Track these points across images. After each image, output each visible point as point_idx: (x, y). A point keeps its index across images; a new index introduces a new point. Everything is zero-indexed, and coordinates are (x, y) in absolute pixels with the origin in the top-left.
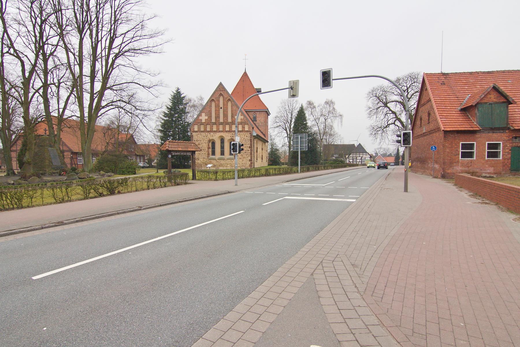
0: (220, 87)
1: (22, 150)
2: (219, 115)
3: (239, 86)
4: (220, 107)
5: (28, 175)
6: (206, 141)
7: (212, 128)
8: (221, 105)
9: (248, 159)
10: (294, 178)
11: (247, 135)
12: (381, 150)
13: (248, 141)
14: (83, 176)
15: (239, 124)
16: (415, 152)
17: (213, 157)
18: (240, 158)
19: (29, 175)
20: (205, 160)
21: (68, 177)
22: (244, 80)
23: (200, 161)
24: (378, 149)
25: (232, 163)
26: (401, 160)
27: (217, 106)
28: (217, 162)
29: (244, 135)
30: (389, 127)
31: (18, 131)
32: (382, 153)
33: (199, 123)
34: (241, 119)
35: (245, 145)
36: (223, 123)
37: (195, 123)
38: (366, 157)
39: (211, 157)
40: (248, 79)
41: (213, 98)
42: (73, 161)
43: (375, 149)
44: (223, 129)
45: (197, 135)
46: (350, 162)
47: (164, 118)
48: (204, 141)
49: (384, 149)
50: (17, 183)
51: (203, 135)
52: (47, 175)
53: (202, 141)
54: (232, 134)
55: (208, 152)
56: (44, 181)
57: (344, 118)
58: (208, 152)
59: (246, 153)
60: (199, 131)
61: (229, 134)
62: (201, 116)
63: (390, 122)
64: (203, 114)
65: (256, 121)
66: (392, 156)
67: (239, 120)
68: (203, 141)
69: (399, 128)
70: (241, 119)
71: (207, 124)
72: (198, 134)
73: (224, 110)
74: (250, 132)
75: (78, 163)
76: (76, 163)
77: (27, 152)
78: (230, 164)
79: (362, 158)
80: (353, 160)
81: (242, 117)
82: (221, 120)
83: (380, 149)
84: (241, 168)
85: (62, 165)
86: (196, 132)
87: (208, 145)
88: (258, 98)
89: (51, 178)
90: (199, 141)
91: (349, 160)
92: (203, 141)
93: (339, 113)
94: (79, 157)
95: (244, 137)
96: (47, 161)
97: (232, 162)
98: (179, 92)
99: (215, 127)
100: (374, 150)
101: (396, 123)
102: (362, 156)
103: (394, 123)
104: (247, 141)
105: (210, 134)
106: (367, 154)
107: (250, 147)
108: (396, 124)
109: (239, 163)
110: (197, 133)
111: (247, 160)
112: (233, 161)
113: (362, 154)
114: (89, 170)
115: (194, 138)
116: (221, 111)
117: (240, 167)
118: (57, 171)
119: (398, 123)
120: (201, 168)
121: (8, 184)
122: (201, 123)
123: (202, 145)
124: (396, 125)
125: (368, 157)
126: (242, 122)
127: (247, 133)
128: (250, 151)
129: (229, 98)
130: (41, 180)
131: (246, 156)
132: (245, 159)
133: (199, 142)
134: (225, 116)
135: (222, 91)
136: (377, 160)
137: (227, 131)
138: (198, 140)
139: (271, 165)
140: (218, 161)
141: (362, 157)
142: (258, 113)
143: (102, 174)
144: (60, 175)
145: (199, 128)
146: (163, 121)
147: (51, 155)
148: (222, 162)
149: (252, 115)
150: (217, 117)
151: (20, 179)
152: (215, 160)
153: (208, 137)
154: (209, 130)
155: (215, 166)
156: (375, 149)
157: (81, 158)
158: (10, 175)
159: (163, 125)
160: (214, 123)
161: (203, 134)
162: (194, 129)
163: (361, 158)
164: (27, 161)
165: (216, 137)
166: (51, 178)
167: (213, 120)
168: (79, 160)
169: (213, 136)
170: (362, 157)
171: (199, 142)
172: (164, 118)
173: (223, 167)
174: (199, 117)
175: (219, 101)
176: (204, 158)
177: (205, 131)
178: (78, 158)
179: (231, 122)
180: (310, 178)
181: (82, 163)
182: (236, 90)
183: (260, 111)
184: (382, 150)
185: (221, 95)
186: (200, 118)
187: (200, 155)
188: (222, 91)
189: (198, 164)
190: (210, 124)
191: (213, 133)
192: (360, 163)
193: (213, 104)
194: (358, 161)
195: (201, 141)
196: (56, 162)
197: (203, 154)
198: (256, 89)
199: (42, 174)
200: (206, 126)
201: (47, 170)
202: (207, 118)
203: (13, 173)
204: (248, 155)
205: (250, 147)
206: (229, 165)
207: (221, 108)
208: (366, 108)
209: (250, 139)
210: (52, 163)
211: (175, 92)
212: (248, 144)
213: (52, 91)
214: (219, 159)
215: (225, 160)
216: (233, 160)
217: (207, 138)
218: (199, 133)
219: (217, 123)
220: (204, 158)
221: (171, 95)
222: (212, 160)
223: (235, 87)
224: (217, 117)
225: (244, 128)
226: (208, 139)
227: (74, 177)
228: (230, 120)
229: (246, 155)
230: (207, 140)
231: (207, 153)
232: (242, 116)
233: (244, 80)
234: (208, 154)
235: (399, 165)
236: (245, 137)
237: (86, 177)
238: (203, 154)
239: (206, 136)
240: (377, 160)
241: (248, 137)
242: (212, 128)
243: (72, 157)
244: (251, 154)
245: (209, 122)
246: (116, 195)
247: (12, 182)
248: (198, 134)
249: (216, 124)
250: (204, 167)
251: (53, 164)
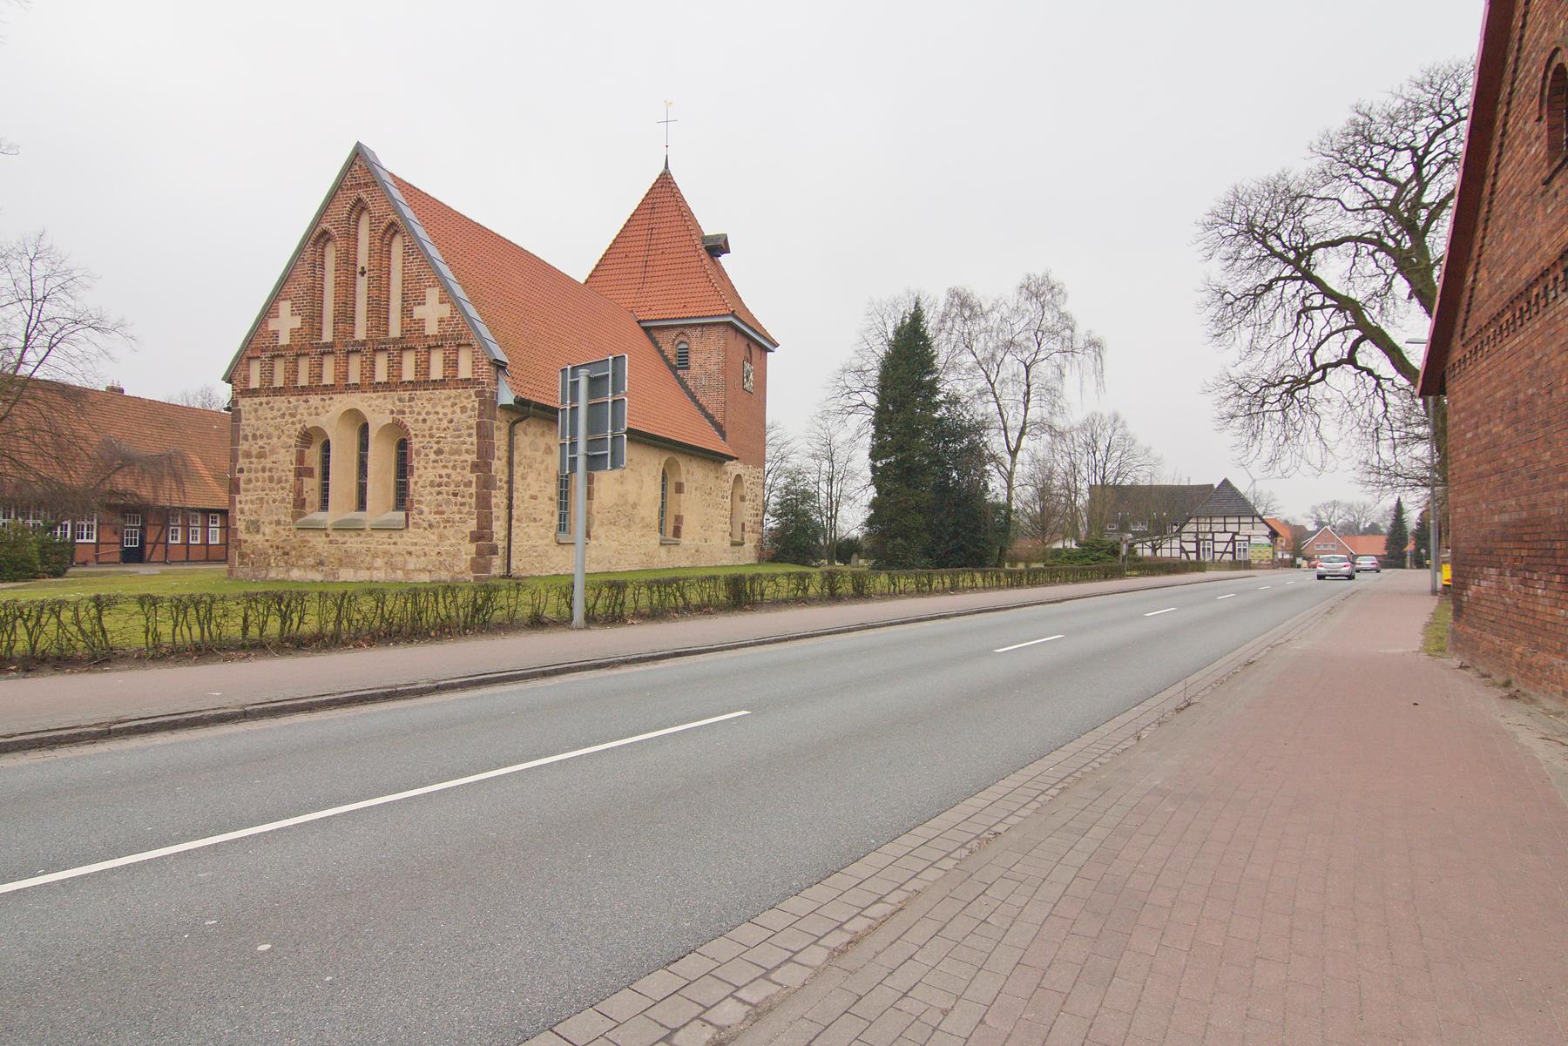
3: (632, 228)
4: (359, 270)
9: (467, 532)
10: (1148, 585)
12: (1336, 512)
13: (470, 435)
15: (430, 347)
16: (1498, 471)
17: (319, 516)
18: (431, 526)
20: (282, 532)
23: (264, 534)
24: (1325, 506)
26: (1410, 547)
27: (348, 260)
28: (331, 542)
29: (454, 405)
30: (1323, 378)
32: (1340, 521)
34: (441, 321)
35: (457, 457)
37: (249, 353)
38: (1254, 532)
43: (1313, 507)
45: (256, 410)
46: (1187, 553)
48: (284, 438)
49: (1350, 508)
51: (279, 410)
54: (400, 400)
55: (299, 492)
57: (1106, 356)
58: (299, 492)
61: (385, 398)
62: (277, 317)
63: (1323, 357)
64: (285, 307)
65: (688, 368)
66: (1381, 533)
67: (432, 329)
69: (1378, 384)
71: (298, 355)
72: (261, 404)
75: (171, 542)
79: (1237, 538)
80: (1198, 545)
81: (446, 310)
83: (1331, 510)
84: (435, 577)
86: (254, 393)
87: (301, 459)
91: (1183, 544)
92: (279, 437)
93: (1089, 332)
95: (448, 410)
97: (395, 543)
100: (1308, 512)
101: (1361, 359)
102: (1234, 528)
103: (1351, 360)
104: (465, 432)
105: (307, 401)
106: (1256, 520)
107: (475, 467)
108: (1360, 364)
109: (427, 549)
112: (399, 540)
113: (1236, 520)
115: (244, 422)
117: (430, 572)
119: (1371, 355)
122: (275, 348)
124: (1362, 369)
125: (1260, 535)
126: (443, 338)
128: (474, 485)
131: (460, 512)
132: (450, 532)
133: (261, 443)
134: (379, 309)
136: (1318, 546)
137: (376, 387)
138: (258, 433)
139: (775, 559)
140: (334, 536)
141: (1237, 533)
142: (697, 332)
148: (353, 543)
149: (668, 342)
152: (323, 534)
153: (298, 417)
155: (321, 563)
156: (1314, 509)
161: (280, 402)
163: (1233, 537)
165: (329, 414)
169: (317, 414)
170: (1237, 533)
171: (261, 443)
173: (356, 568)
177: (291, 389)
180: (919, 624)
181: (94, 541)
182: (619, 245)
183: (703, 325)
184: (1341, 513)
187: (265, 505)
189: (253, 553)
192: (1228, 557)
194: (1219, 547)
195: (269, 437)
197: (274, 501)
198: (704, 239)
205: (475, 467)
206: (379, 562)
208: (1206, 296)
209: (479, 425)
212: (467, 451)
214: (341, 528)
215: (364, 534)
218: (264, 400)
220: (278, 523)
222: (311, 533)
223: (618, 232)
224: (345, 315)
226: (298, 426)
229: (455, 509)
231: (291, 494)
234: (300, 503)
235: (1404, 567)
236: (453, 413)
239: (292, 415)
240: (1318, 546)
241: (469, 413)
244: (484, 502)
246: (96, 675)
248: (261, 404)
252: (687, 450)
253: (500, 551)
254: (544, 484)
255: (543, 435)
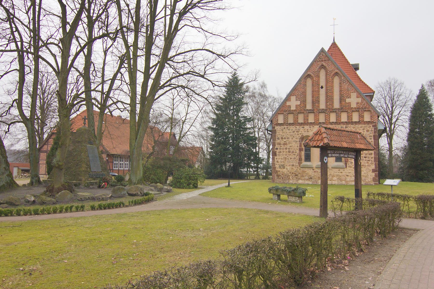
0: (321, 55)
1: (52, 149)
2: (318, 97)
5: (56, 186)
6: (297, 138)
7: (306, 118)
8: (322, 82)
11: (368, 129)
14: (135, 191)
15: (353, 111)
17: (308, 163)
19: (58, 186)
21: (114, 192)
22: (333, 54)
23: (287, 169)
25: (340, 174)
27: (316, 87)
28: (315, 172)
29: (363, 129)
31: (52, 129)
33: (286, 111)
34: (357, 103)
36: (326, 110)
37: (279, 112)
39: (304, 163)
40: (339, 52)
41: (309, 73)
42: (108, 165)
44: (326, 119)
45: (282, 130)
47: (216, 112)
48: (294, 139)
50: (40, 200)
51: (292, 130)
52: (82, 187)
53: (290, 139)
55: (300, 156)
56: (79, 199)
59: (367, 159)
60: (286, 123)
64: (293, 98)
68: (292, 139)
70: (357, 103)
73: (327, 90)
74: (374, 124)
75: (114, 169)
76: (111, 168)
77: (59, 150)
78: (337, 175)
82: (322, 106)
85: (102, 172)
88: (357, 77)
89: (88, 194)
90: (285, 138)
92: (292, 139)
94: (115, 161)
96: (84, 165)
97: (341, 172)
98: (236, 78)
99: (311, 118)
105: (303, 127)
110: (282, 127)
111: (368, 170)
112: (343, 171)
114: (138, 180)
115: (277, 133)
116: (323, 92)
118: (95, 181)
120: (287, 181)
121: (26, 202)
123: (290, 145)
127: (368, 126)
128: (373, 154)
129: (336, 71)
130: (74, 195)
131: (368, 163)
133: (285, 140)
134: (329, 98)
135: (325, 61)
143: (160, 187)
144: (100, 187)
145: (286, 119)
146: (214, 117)
147: (89, 155)
150: (316, 101)
151: (45, 193)
153: (300, 132)
154: (303, 122)
155: (311, 178)
157: (117, 162)
158: (34, 183)
159: (214, 122)
160: (310, 110)
161: (293, 128)
162: (277, 120)
164: (58, 164)
166: (88, 194)
167: (309, 107)
168: (120, 164)
169: (308, 132)
171: (285, 140)
172: (216, 112)
174: (286, 103)
175: (318, 77)
176: (293, 165)
177: (295, 123)
178: (114, 162)
179: (338, 109)
185: (323, 67)
186: (288, 103)
187: (287, 160)
188: (325, 61)
189: (283, 175)
190: (303, 113)
191: (308, 126)
193: (309, 82)
195: (288, 138)
196: (96, 168)
197: (291, 159)
199: (75, 185)
200: (297, 115)
201: (84, 179)
202: (298, 103)
203: (39, 181)
204: (370, 162)
206: (335, 178)
207: (322, 87)
210: (90, 169)
211: (231, 78)
213: (94, 69)
216: (342, 169)
217: (298, 134)
218: (286, 127)
219: (315, 110)
220: (293, 165)
221: (226, 82)
222: (307, 169)
224: (316, 101)
225: (363, 117)
226: (300, 135)
227: (122, 193)
228: (336, 105)
229: (366, 162)
230: (298, 137)
232: (358, 99)
233: (333, 54)
234: (300, 159)
237: (139, 193)
238: (291, 159)
239: (297, 132)
241: (370, 132)
242: (306, 118)
243: (108, 160)
245: (302, 109)
247: (33, 199)
248: (284, 128)
249: (314, 112)
250: (293, 179)
251: (92, 170)
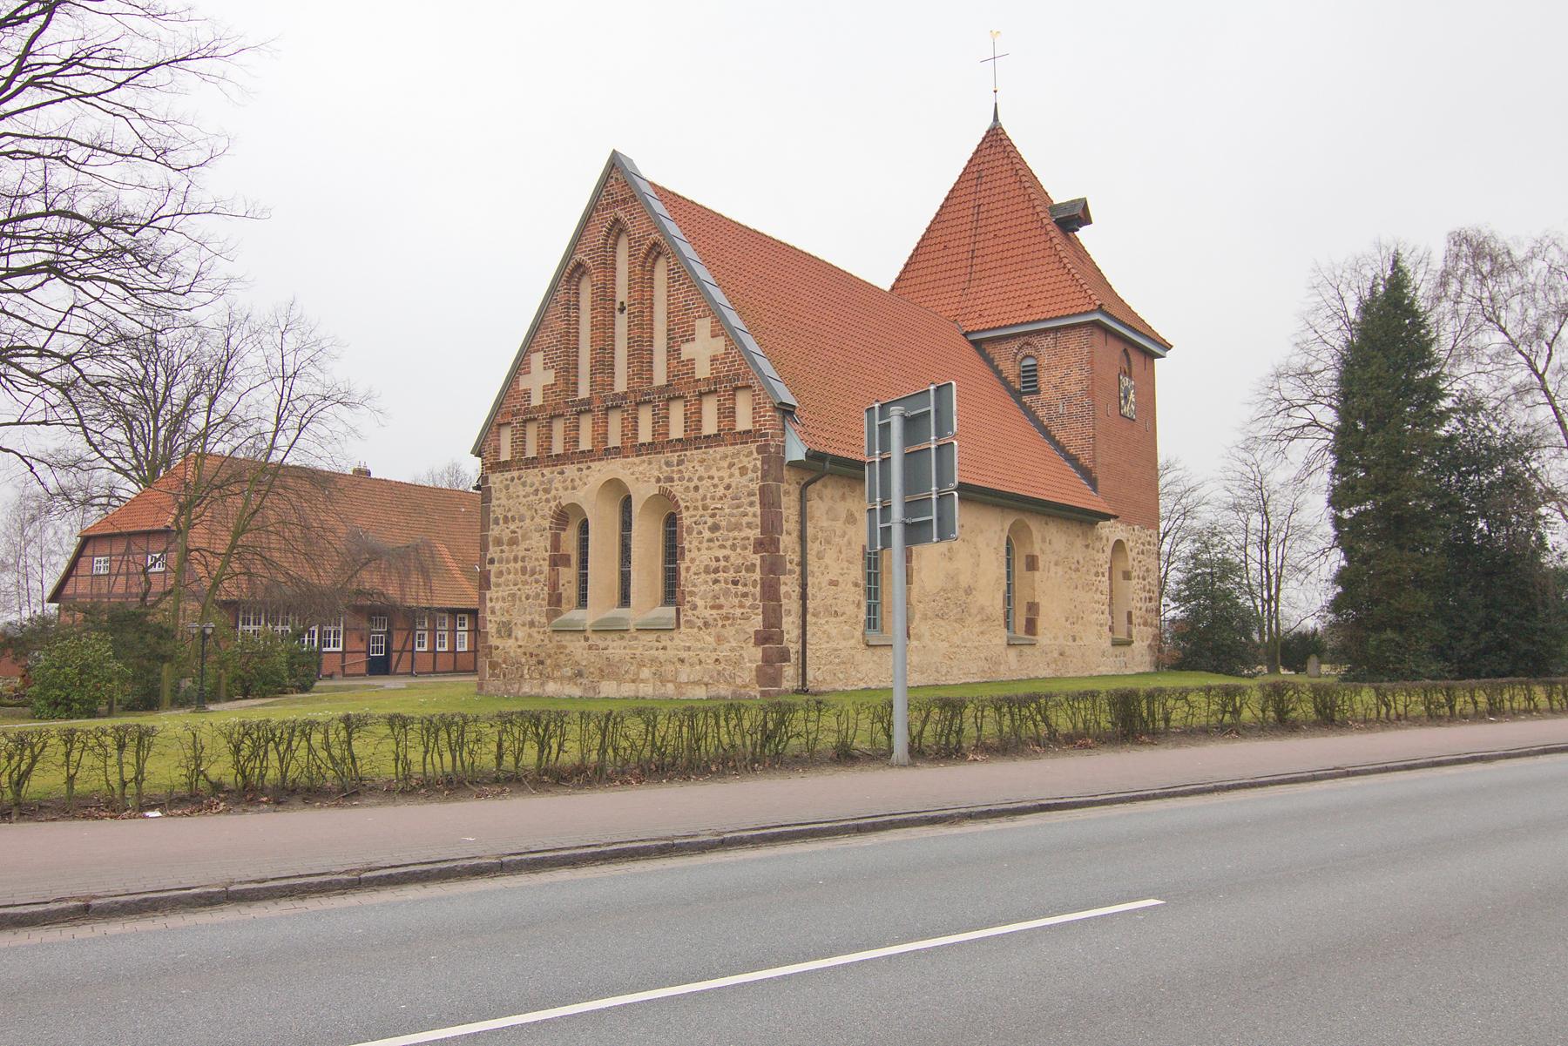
252: (1074, 515)
253: (793, 657)
254: (845, 564)
255: (843, 498)
